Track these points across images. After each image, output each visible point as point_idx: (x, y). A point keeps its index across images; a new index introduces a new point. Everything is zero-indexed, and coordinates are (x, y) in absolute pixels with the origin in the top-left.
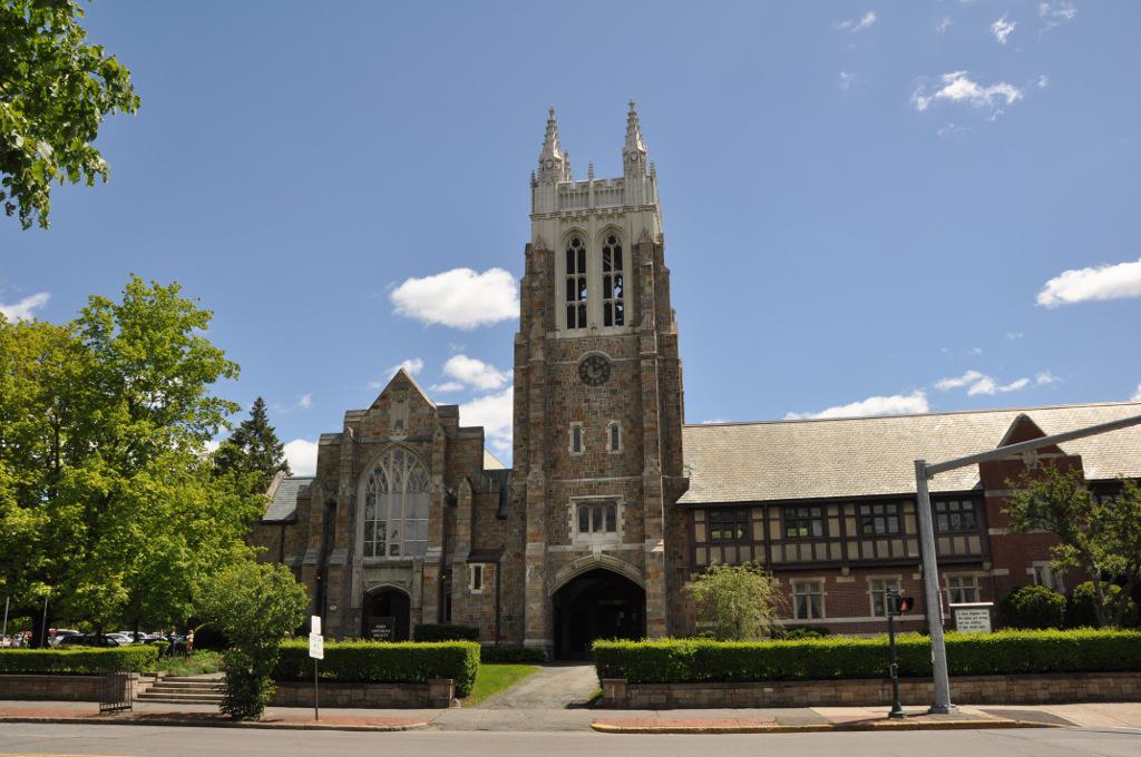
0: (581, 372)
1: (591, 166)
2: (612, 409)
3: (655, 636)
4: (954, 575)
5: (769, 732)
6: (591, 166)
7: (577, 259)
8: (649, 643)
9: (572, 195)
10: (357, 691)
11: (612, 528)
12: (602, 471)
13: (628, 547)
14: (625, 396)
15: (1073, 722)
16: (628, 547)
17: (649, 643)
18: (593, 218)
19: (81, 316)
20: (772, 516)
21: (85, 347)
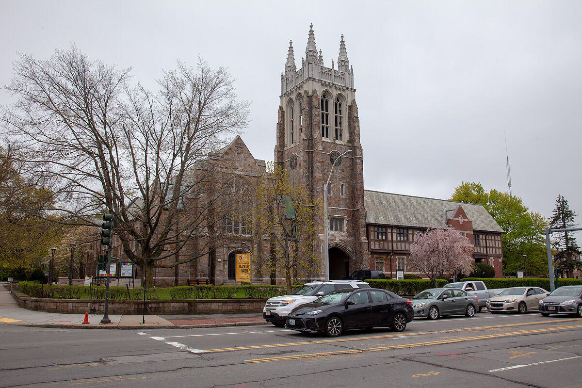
0: (331, 159)
1: (333, 61)
2: (342, 178)
3: (497, 277)
4: (400, 257)
5: (252, 325)
6: (333, 61)
7: (324, 104)
8: (494, 279)
9: (325, 73)
10: (63, 285)
11: (341, 230)
12: (339, 205)
13: (348, 239)
14: (347, 172)
15: (295, 337)
16: (348, 239)
17: (494, 279)
18: (333, 87)
19: (60, 51)
20: (393, 231)
21: (568, 248)
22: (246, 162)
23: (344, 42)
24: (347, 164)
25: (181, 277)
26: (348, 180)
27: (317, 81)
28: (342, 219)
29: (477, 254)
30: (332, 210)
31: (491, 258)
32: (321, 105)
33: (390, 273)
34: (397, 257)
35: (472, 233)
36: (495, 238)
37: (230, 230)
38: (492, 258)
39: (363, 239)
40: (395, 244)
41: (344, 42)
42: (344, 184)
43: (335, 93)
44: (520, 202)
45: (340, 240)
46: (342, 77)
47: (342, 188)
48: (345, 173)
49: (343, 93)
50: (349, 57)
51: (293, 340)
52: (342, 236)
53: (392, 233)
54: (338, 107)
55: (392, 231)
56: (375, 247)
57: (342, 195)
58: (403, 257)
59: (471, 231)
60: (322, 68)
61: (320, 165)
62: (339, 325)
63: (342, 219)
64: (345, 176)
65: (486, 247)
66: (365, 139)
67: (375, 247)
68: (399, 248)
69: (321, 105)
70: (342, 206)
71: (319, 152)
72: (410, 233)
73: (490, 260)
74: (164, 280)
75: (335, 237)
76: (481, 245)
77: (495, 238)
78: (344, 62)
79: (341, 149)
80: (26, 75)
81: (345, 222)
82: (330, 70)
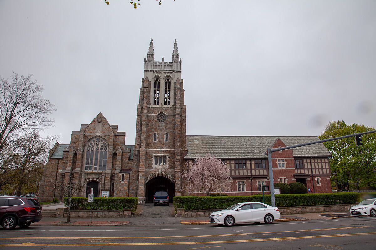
12: (162, 147)
13: (170, 170)
16: (170, 170)
18: (163, 73)
22: (104, 127)
23: (177, 44)
24: (171, 120)
25: (137, 194)
26: (171, 130)
27: (150, 71)
28: (165, 157)
29: (301, 175)
30: (157, 151)
31: (317, 177)
32: (162, 87)
33: (251, 192)
34: (257, 180)
35: (293, 158)
36: (314, 161)
37: (91, 168)
38: (319, 177)
39: (178, 169)
40: (314, 171)
41: (177, 44)
42: (168, 133)
43: (163, 76)
44: (342, 124)
45: (162, 171)
46: (176, 65)
47: (167, 136)
48: (168, 126)
49: (171, 75)
50: (180, 52)
51: (257, 220)
52: (165, 168)
53: (251, 164)
54: (168, 85)
55: (310, 161)
56: (239, 174)
57: (166, 140)
58: (244, 180)
59: (291, 157)
60: (155, 63)
61: (144, 122)
62: (227, 222)
63: (165, 157)
64: (169, 128)
65: (311, 169)
66: (187, 102)
67: (239, 174)
68: (257, 174)
69: (162, 87)
70: (165, 148)
71: (144, 114)
72: (248, 162)
73: (316, 179)
74: (47, 198)
75: (158, 169)
76: (306, 167)
77: (314, 161)
78: (176, 56)
79: (166, 110)
80: (19, 108)
81: (167, 159)
82: (161, 63)
